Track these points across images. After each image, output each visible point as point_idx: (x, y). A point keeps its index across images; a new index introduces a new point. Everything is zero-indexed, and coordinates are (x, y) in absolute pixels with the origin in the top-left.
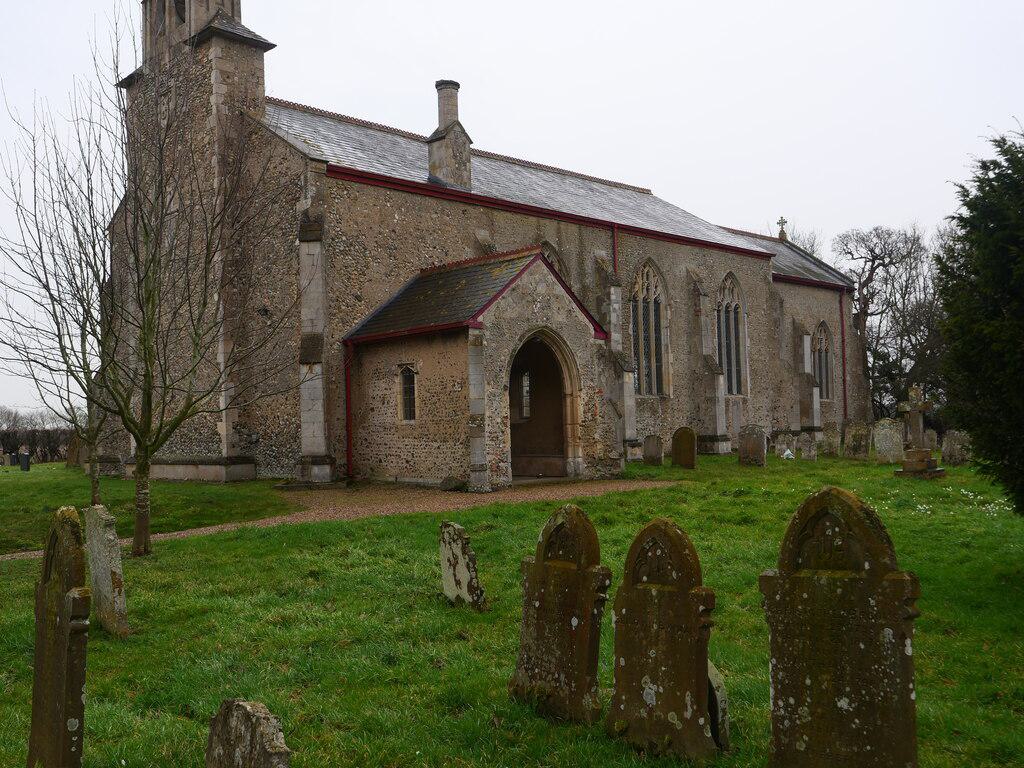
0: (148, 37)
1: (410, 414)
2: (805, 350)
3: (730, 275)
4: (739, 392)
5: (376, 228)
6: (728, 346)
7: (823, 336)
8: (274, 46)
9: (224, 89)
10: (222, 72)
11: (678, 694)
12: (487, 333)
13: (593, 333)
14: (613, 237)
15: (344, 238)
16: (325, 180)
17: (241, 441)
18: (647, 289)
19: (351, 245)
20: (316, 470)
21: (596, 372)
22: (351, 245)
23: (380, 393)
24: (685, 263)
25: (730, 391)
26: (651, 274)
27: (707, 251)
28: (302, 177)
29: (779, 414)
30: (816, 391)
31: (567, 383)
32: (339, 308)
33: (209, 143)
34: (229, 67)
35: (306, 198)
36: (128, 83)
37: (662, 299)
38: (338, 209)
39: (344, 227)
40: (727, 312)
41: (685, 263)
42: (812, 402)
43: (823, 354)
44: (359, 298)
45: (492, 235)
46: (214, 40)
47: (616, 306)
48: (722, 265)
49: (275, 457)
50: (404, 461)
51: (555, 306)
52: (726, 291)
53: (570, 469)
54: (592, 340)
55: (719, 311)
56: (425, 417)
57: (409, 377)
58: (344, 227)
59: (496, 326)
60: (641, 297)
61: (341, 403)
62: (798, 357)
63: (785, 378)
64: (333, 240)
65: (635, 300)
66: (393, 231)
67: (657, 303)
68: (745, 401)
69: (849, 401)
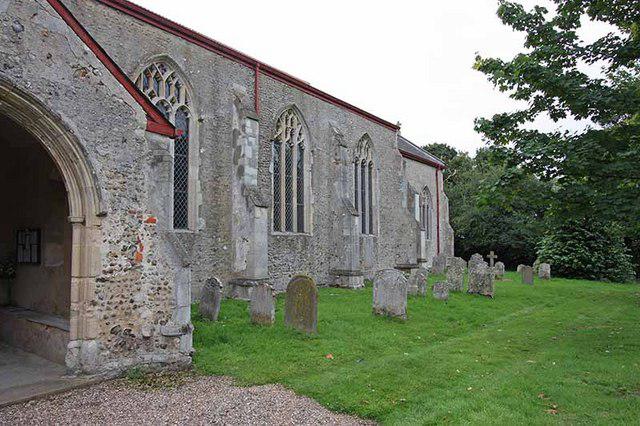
3: (366, 136)
4: (289, 228)
6: (363, 194)
13: (144, 121)
21: (145, 188)
24: (329, 118)
25: (363, 231)
27: (347, 112)
30: (423, 234)
31: (74, 202)
37: (307, 146)
40: (363, 167)
41: (329, 118)
48: (361, 127)
52: (363, 150)
54: (140, 133)
55: (356, 165)
60: (284, 140)
62: (411, 209)
63: (406, 223)
65: (277, 142)
68: (375, 240)
69: (441, 241)
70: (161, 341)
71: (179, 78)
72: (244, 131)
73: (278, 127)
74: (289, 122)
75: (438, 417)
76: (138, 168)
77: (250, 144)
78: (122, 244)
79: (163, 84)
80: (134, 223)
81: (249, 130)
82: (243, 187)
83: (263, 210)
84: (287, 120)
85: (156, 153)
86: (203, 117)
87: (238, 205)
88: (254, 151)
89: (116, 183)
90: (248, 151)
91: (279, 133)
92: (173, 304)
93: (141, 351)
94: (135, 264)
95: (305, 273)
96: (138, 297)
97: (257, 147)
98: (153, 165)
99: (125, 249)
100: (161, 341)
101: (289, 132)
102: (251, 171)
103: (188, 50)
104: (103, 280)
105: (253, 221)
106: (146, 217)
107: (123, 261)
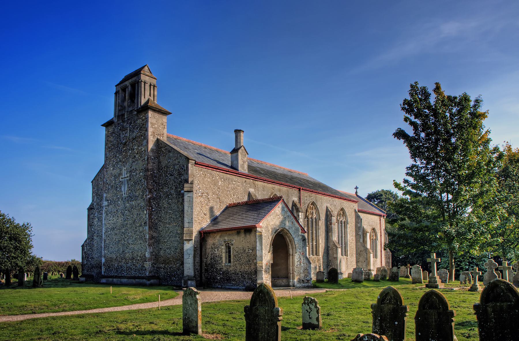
0: (117, 108)
7: (374, 234)
8: (102, 125)
17: (154, 270)
28: (185, 166)
29: (359, 264)
31: (291, 250)
33: (144, 151)
36: (108, 125)
46: (149, 110)
49: (169, 277)
53: (291, 284)
61: (198, 256)
64: (197, 191)
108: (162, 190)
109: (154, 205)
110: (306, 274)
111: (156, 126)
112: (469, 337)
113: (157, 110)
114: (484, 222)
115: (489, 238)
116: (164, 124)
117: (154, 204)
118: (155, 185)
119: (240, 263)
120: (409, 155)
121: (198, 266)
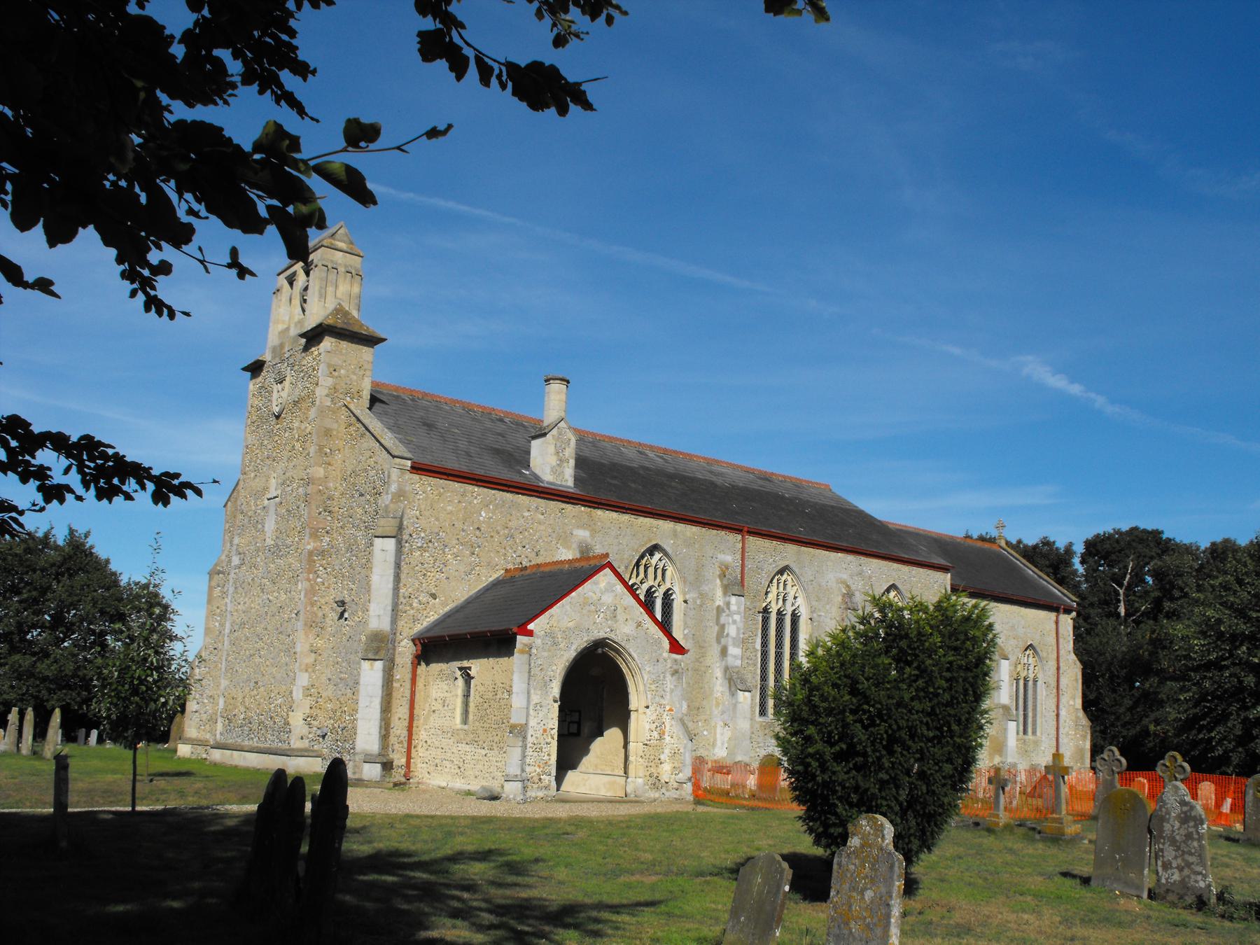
1: (465, 721)
2: (363, 702)
5: (459, 525)
8: (386, 339)
9: (330, 382)
10: (329, 365)
11: (1204, 766)
12: (538, 642)
14: (743, 540)
15: (423, 535)
16: (408, 476)
18: (784, 600)
19: (430, 541)
20: (367, 766)
21: (668, 689)
22: (430, 541)
23: (442, 695)
26: (789, 583)
32: (411, 605)
34: (336, 360)
35: (387, 494)
38: (419, 505)
39: (423, 523)
42: (1006, 738)
43: (1030, 683)
44: (434, 596)
45: (592, 536)
47: (737, 617)
50: (456, 767)
51: (621, 616)
54: (666, 655)
56: (477, 724)
57: (468, 678)
58: (423, 523)
59: (550, 634)
64: (411, 535)
66: (478, 528)
67: (795, 618)
70: (676, 785)
71: (665, 560)
72: (729, 609)
73: (767, 593)
74: (781, 585)
75: (785, 755)
76: (664, 677)
77: (734, 622)
78: (656, 724)
79: (651, 570)
80: (662, 711)
81: (734, 608)
82: (726, 669)
83: (747, 693)
84: (778, 583)
85: (675, 667)
86: (687, 597)
87: (719, 686)
88: (738, 629)
89: (653, 687)
90: (732, 630)
91: (768, 600)
92: (683, 763)
93: (663, 790)
94: (661, 738)
95: (338, 755)
96: (662, 757)
97: (741, 625)
98: (673, 675)
99: (657, 727)
100: (676, 785)
101: (781, 597)
102: (734, 651)
103: (675, 531)
104: (646, 745)
105: (735, 706)
106: (668, 708)
107: (655, 734)
108: (341, 531)
109: (321, 568)
110: (676, 765)
111: (343, 372)
112: (1072, 939)
113: (347, 333)
114: (272, 656)
115: (904, 789)
116: (366, 366)
117: (321, 566)
118: (329, 518)
119: (485, 725)
120: (351, 118)
121: (402, 729)
